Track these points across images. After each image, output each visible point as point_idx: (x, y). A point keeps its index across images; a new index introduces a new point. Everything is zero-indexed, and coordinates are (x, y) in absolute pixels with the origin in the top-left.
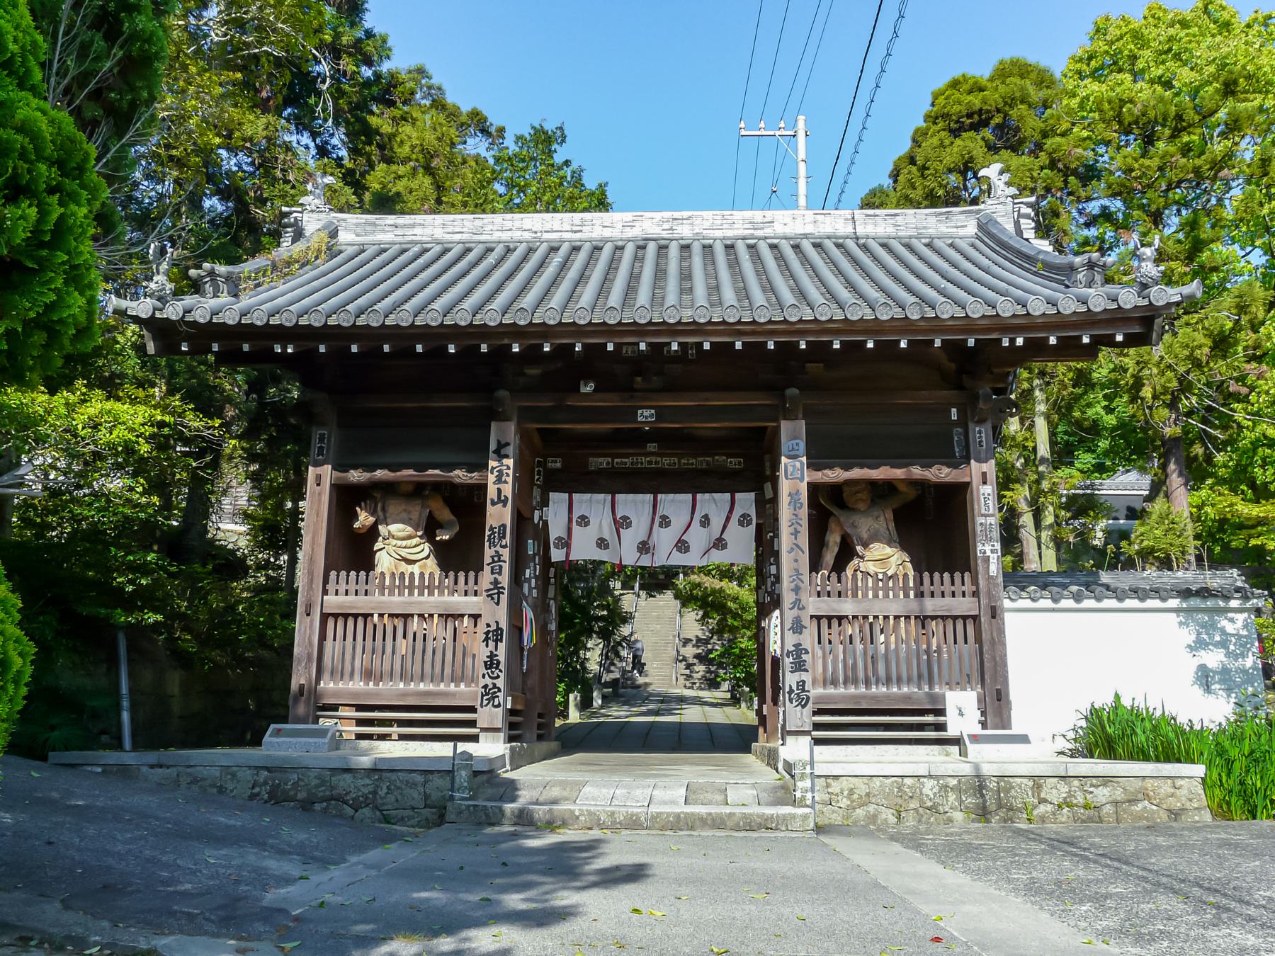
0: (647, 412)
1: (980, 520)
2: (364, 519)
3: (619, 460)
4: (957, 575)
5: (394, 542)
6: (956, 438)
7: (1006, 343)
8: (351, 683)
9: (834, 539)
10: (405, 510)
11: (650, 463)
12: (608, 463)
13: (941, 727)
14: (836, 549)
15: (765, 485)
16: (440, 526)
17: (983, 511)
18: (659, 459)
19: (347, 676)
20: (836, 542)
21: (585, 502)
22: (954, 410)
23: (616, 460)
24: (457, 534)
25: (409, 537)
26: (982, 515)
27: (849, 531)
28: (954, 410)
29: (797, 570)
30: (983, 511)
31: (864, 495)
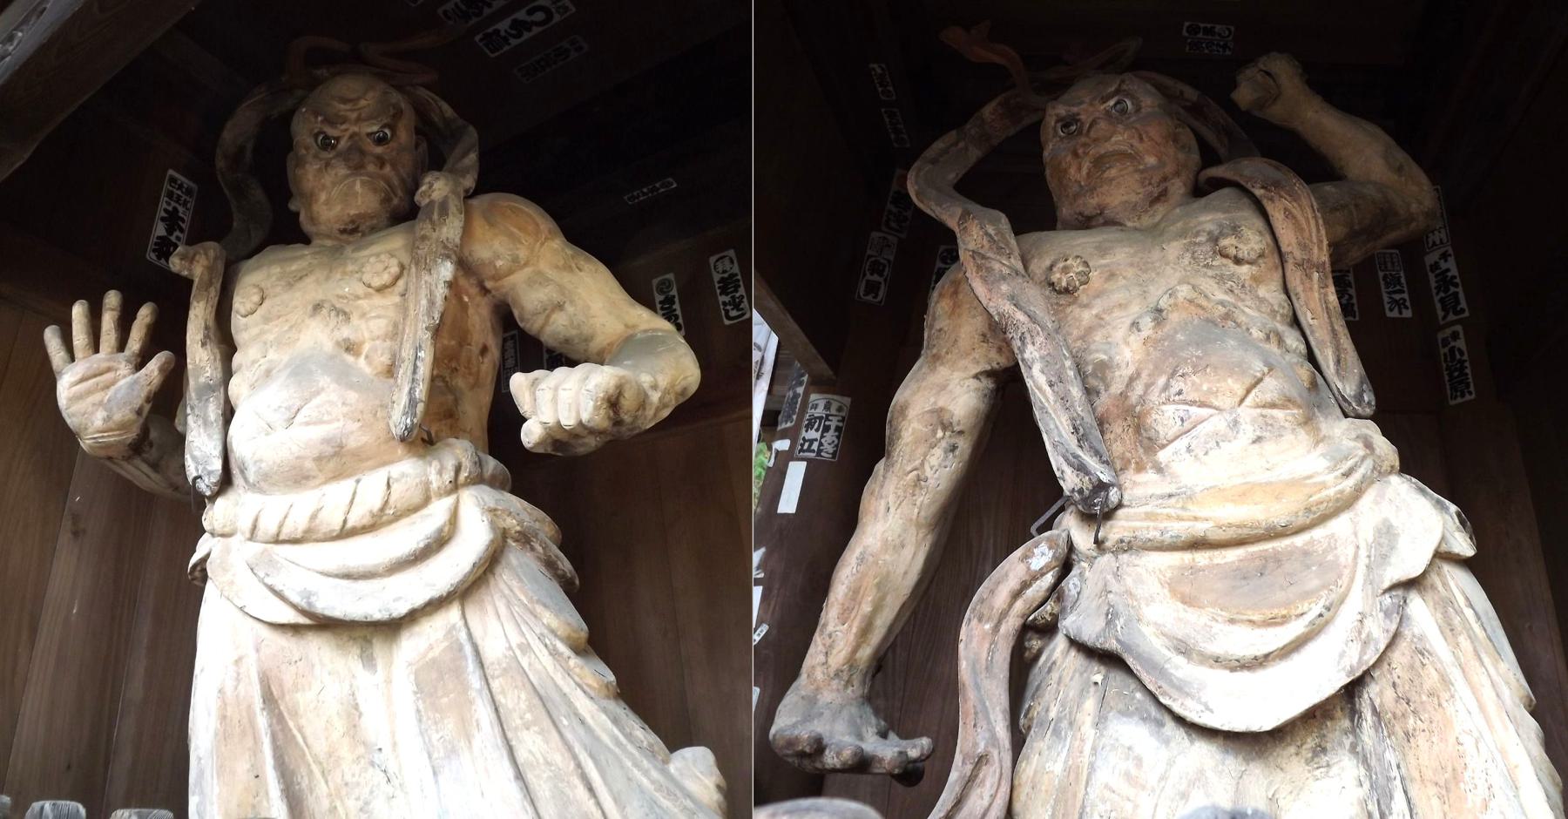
20: (941, 420)
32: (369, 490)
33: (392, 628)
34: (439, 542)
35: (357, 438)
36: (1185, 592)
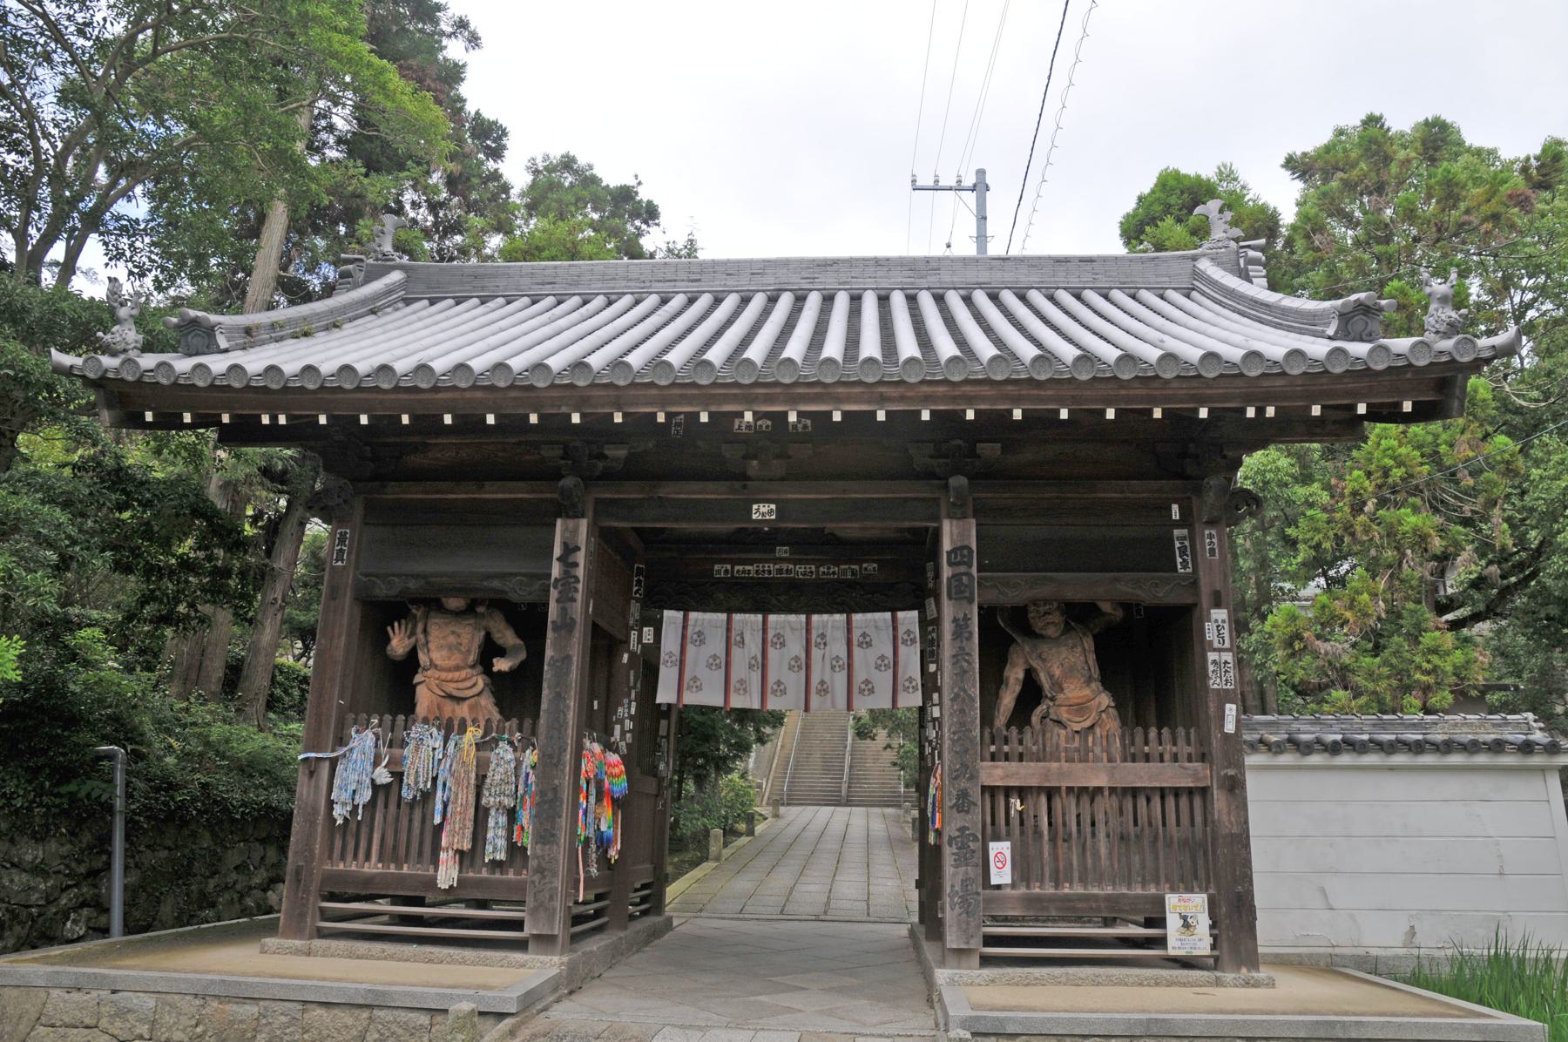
0: (764, 508)
1: (1212, 656)
2: (398, 644)
3: (741, 568)
4: (1181, 731)
5: (437, 674)
6: (1177, 544)
7: (1251, 412)
8: (367, 864)
9: (1015, 675)
10: (453, 633)
11: (780, 571)
12: (726, 571)
13: (1161, 942)
14: (1018, 689)
15: (927, 602)
16: (501, 652)
17: (1216, 645)
18: (791, 566)
19: (350, 856)
20: (1017, 679)
21: (708, 621)
22: (1175, 508)
23: (737, 568)
24: (522, 664)
25: (458, 668)
26: (1215, 650)
27: (1034, 664)
28: (1175, 508)
29: (963, 724)
30: (1216, 645)
31: (1056, 617)
32: (463, 674)
33: (464, 699)
34: (474, 685)
35: (462, 664)
36: (1068, 712)
